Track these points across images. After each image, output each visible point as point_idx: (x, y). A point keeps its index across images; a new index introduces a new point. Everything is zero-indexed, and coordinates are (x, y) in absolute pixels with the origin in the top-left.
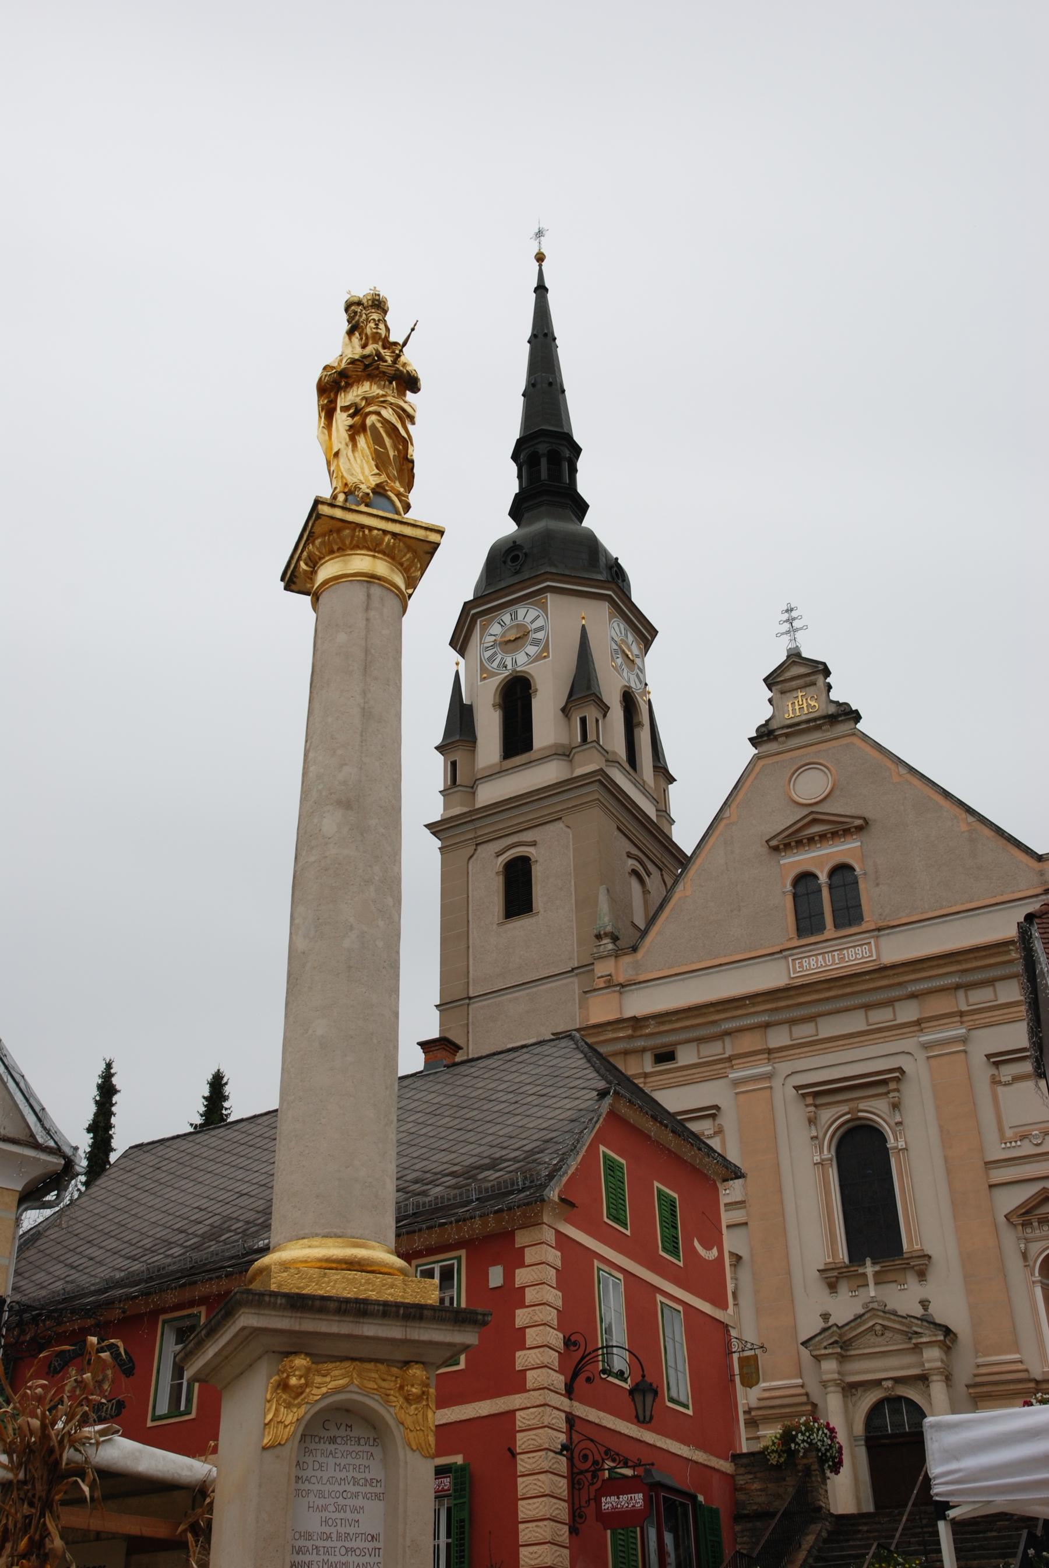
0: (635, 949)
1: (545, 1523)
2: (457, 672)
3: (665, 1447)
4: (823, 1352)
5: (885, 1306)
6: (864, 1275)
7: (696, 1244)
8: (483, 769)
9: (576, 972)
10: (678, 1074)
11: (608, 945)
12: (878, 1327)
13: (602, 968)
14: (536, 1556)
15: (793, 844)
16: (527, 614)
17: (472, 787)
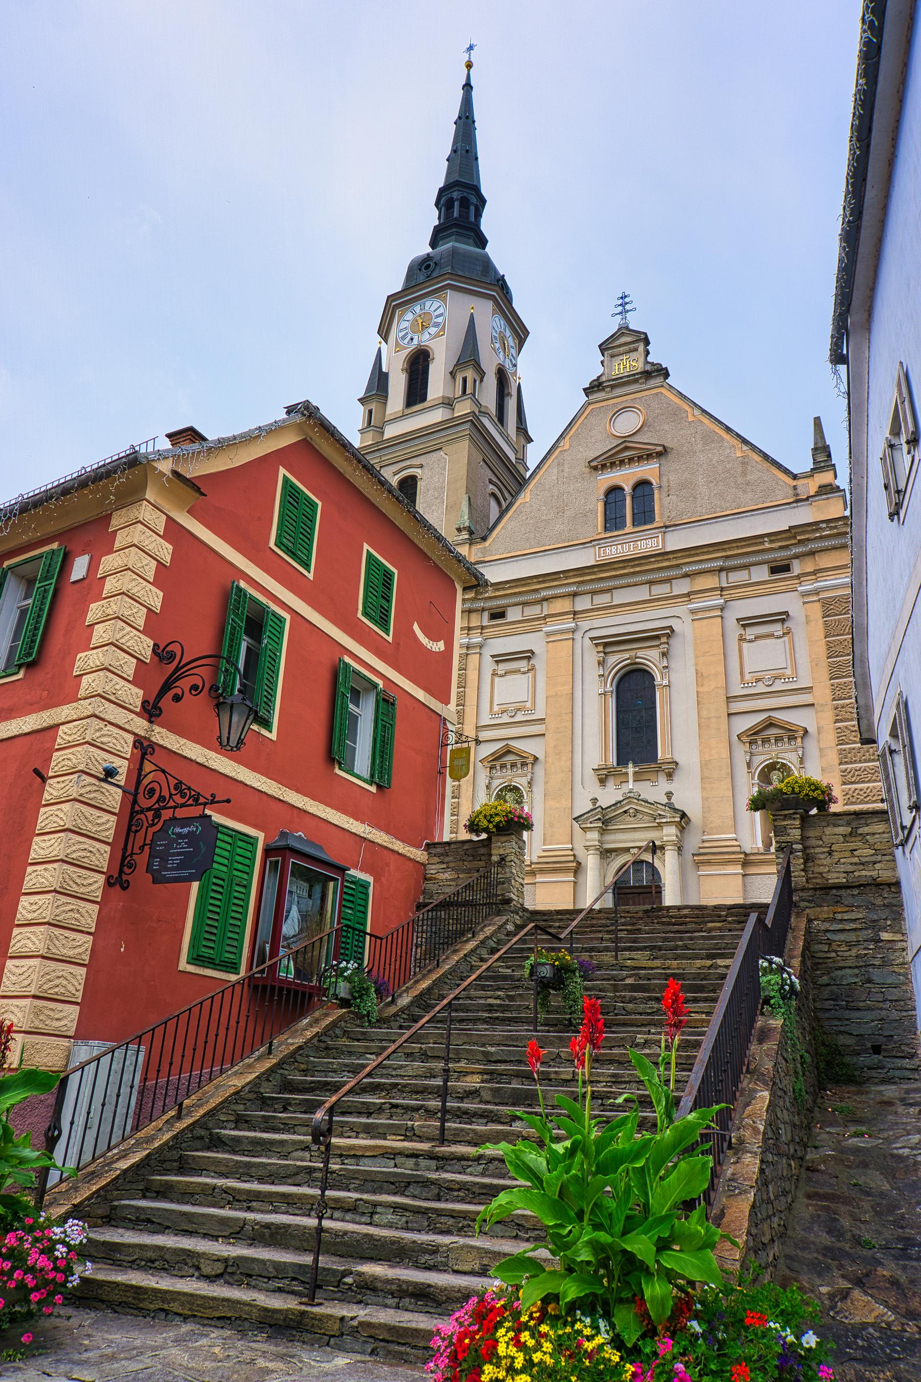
0: (484, 539)
1: (55, 865)
2: (379, 349)
3: (323, 815)
4: (589, 825)
6: (627, 774)
7: (416, 627)
11: (465, 535)
12: (631, 811)
14: (35, 907)
16: (432, 305)
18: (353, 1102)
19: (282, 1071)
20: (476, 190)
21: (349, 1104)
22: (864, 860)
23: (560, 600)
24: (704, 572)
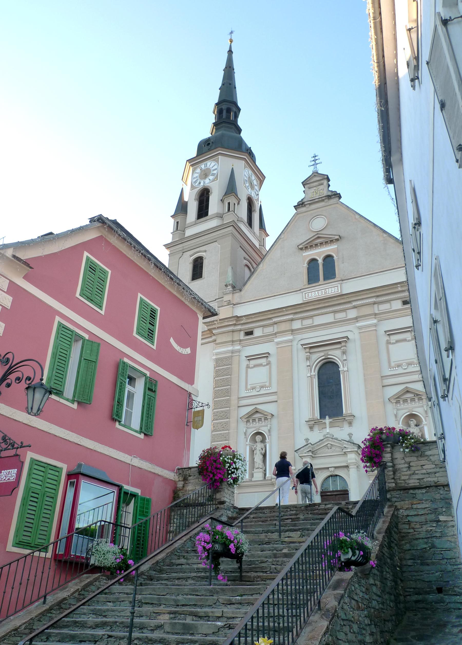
5: (333, 436)
6: (325, 423)
7: (172, 340)
8: (189, 223)
9: (217, 300)
10: (254, 340)
11: (230, 288)
12: (329, 445)
13: (227, 298)
15: (309, 247)
16: (211, 164)
17: (184, 231)
18: (86, 634)
19: (49, 615)
20: (235, 104)
21: (84, 635)
22: (429, 471)
23: (284, 324)
24: (366, 305)
